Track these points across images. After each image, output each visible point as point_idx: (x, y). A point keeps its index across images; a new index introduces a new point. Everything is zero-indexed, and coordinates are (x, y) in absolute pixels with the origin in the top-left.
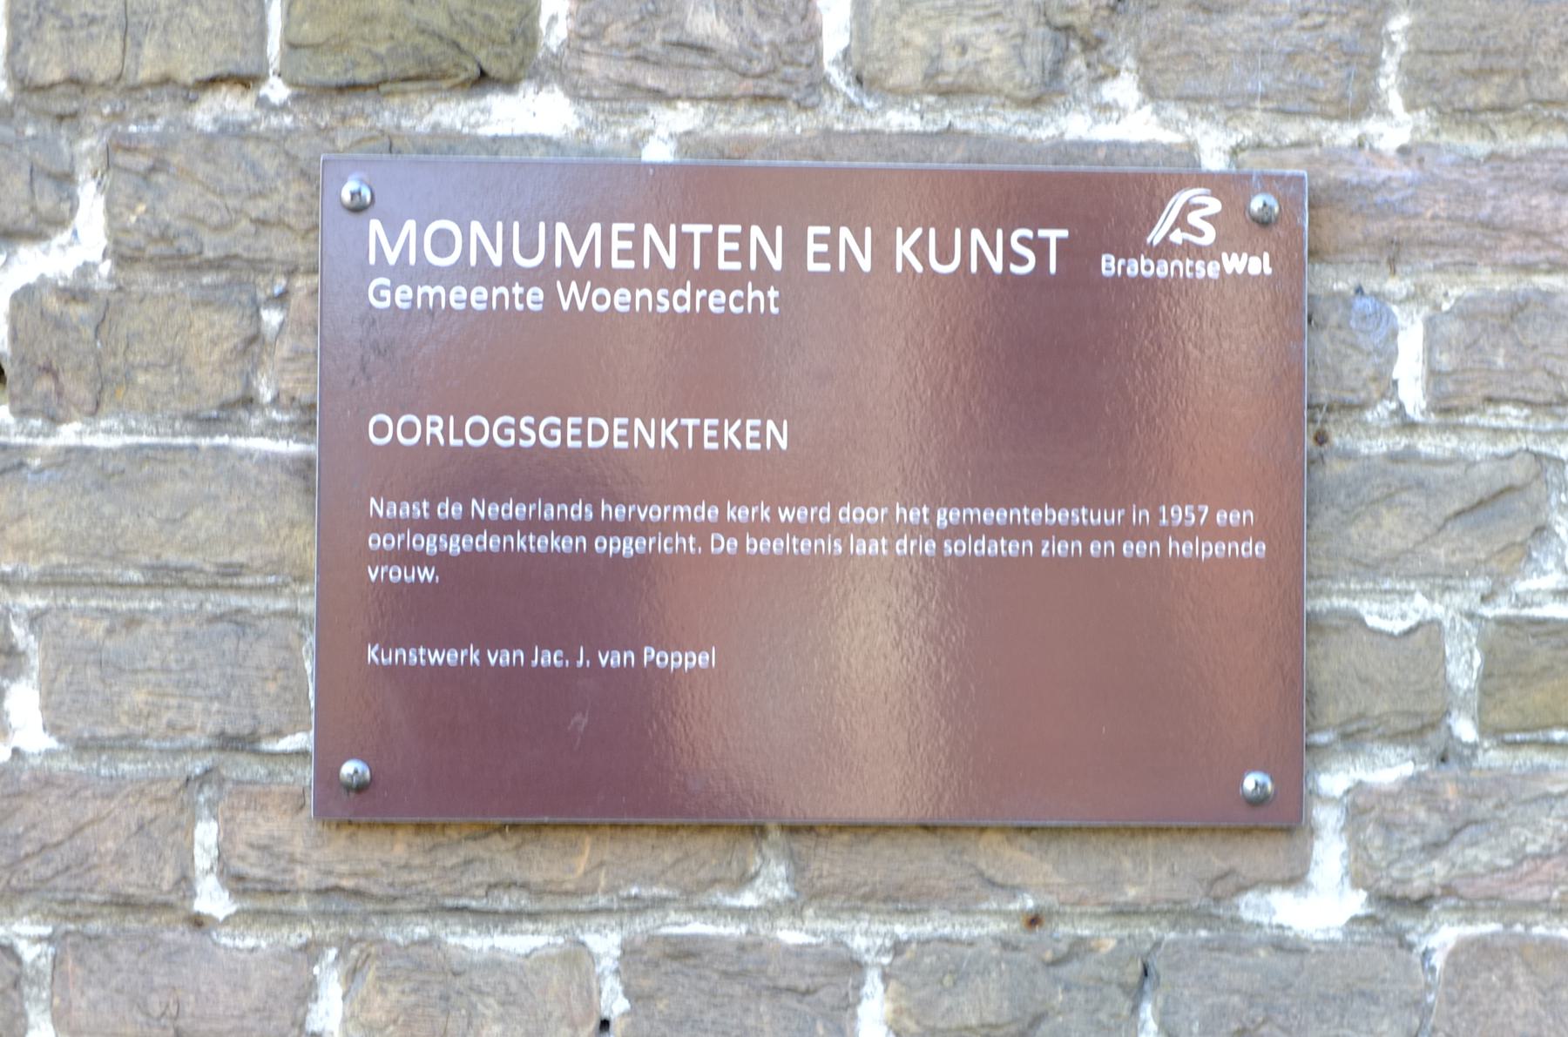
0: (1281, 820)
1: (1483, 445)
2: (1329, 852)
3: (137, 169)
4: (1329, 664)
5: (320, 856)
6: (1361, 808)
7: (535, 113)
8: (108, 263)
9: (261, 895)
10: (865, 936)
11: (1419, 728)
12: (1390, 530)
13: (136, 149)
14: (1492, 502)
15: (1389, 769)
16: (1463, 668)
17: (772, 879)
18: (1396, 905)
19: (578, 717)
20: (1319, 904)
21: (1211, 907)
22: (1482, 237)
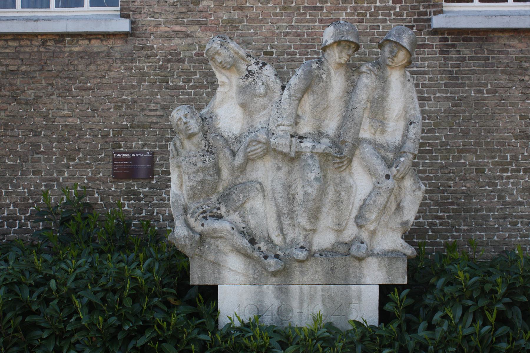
0: (153, 178)
1: (161, 163)
2: (155, 180)
3: (105, 152)
4: (155, 172)
5: (113, 180)
6: (156, 178)
7: (122, 149)
8: (510, 317)
9: (111, 182)
10: (135, 183)
11: (158, 174)
12: (157, 166)
13: (264, 199)
14: (161, 165)
15: (157, 176)
16: (160, 172)
17: (131, 181)
18: (157, 182)
19: (430, 348)
20: (154, 182)
21: (150, 182)
22: (161, 154)
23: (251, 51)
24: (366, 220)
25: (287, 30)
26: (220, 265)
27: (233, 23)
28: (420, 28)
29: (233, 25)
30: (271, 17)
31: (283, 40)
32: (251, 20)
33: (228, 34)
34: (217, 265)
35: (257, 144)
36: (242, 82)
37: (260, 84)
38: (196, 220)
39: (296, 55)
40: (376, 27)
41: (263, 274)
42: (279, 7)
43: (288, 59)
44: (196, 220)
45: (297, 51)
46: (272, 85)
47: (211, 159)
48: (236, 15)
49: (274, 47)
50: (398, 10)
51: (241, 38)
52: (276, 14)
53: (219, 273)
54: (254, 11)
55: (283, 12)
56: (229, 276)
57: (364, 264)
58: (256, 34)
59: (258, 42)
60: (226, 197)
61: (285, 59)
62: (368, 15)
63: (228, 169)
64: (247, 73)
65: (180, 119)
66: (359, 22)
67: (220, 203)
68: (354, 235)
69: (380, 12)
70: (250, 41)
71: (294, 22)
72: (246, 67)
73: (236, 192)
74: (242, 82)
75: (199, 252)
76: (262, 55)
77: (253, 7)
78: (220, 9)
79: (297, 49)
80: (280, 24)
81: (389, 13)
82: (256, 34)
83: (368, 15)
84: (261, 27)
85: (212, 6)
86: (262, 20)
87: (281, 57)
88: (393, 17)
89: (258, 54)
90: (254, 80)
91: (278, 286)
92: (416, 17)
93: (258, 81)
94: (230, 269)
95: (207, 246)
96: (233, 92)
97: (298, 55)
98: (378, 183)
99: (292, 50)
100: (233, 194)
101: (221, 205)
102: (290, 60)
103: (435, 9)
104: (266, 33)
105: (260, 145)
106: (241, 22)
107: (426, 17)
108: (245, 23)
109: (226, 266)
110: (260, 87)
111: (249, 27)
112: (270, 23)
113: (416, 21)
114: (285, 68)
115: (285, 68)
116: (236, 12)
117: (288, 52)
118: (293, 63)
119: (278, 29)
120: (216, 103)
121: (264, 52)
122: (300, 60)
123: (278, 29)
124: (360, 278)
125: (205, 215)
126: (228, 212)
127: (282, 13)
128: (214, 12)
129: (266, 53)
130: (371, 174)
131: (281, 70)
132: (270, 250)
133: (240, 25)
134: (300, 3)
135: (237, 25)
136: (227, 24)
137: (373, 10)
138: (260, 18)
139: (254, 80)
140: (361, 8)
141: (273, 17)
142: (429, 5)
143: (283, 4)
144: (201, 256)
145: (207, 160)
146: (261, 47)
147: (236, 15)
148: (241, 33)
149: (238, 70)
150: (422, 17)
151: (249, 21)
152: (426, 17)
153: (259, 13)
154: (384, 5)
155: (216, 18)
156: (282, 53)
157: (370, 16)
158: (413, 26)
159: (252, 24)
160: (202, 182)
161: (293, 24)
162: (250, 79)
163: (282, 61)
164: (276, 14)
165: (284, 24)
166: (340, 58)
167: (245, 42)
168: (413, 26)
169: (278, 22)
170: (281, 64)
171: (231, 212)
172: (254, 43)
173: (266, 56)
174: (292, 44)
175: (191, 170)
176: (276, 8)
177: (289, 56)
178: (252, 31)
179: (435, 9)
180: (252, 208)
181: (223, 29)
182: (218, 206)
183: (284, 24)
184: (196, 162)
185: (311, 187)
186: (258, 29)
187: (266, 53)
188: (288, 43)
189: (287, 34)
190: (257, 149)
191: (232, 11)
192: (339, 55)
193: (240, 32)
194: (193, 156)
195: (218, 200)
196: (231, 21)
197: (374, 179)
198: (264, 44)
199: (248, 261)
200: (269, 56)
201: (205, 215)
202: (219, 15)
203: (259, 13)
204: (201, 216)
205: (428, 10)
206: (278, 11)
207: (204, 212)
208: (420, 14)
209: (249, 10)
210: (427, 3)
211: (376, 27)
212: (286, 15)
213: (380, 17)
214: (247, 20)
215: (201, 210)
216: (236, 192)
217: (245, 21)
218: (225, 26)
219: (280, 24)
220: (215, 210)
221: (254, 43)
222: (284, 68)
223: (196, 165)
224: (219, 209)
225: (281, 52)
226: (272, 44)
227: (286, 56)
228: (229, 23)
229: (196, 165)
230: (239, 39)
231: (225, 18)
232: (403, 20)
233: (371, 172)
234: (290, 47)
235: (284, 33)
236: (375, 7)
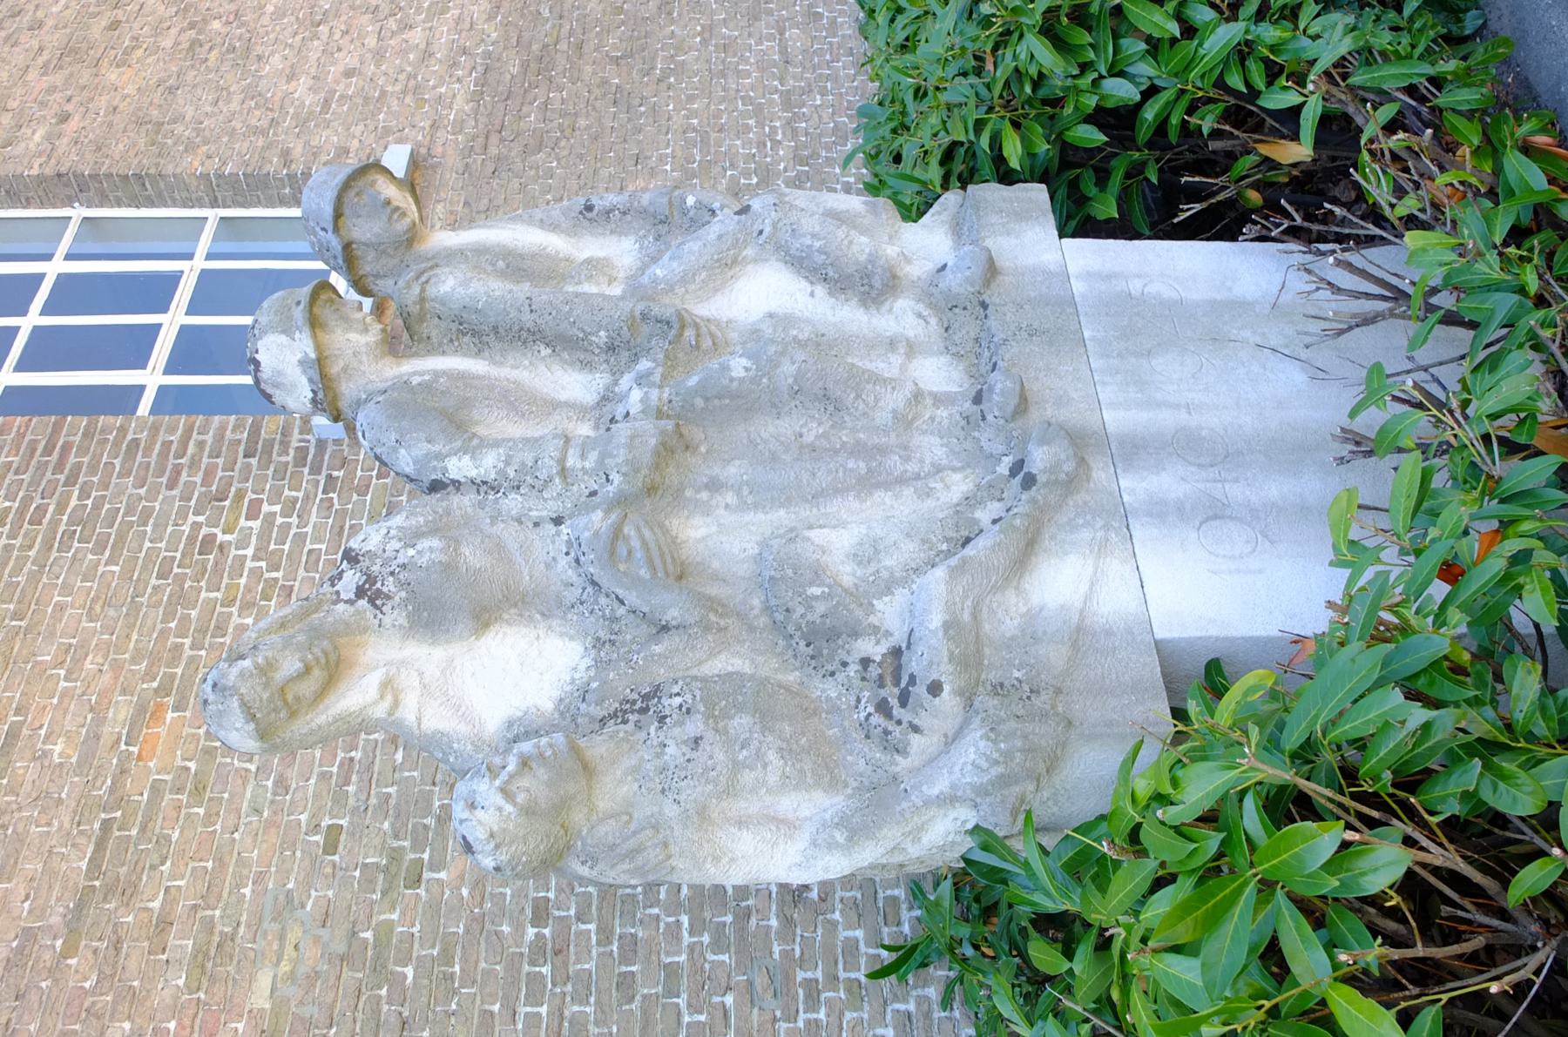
23: (313, 893)
24: (873, 259)
25: (270, 784)
26: (1079, 629)
27: (206, 955)
28: (338, 463)
29: (212, 954)
30: (215, 831)
31: (299, 795)
32: (209, 896)
33: (239, 971)
34: (1082, 636)
35: (627, 539)
36: (394, 616)
37: (411, 552)
38: (915, 729)
39: (352, 759)
40: (313, 557)
41: (1085, 503)
42: (189, 806)
43: (361, 780)
44: (915, 729)
45: (341, 755)
46: (421, 519)
47: (676, 689)
48: (183, 944)
49: (314, 822)
50: (277, 508)
51: (265, 925)
52: (210, 818)
53: (1109, 633)
54: (181, 883)
55: (208, 794)
56: (1115, 599)
57: (1003, 262)
58: (259, 879)
59: (289, 872)
60: (821, 640)
61: (360, 790)
62: (274, 575)
63: (712, 655)
64: (363, 603)
65: (505, 792)
66: (290, 595)
67: (845, 664)
68: (921, 307)
69: (272, 547)
70: (281, 898)
71: (247, 765)
72: (341, 607)
73: (800, 610)
74: (394, 616)
75: (1044, 697)
76: (336, 858)
77: (167, 889)
78: (146, 998)
79: (335, 756)
80: (245, 804)
81: (280, 527)
82: (259, 879)
83: (274, 575)
84: (241, 862)
85: (127, 1025)
86: (221, 862)
87: (352, 802)
88: (294, 520)
89: (329, 870)
90: (392, 573)
91: (1119, 465)
92: (306, 470)
93: (401, 560)
94: (1087, 598)
95: (1017, 674)
96: (426, 656)
97: (353, 754)
98: (761, 232)
99: (335, 770)
100: (809, 617)
101: (849, 660)
102: (366, 777)
103: (296, 431)
104: (265, 846)
105: (629, 530)
106: (209, 925)
107: (312, 451)
108: (217, 912)
109: (1078, 604)
110: (419, 552)
111: (234, 898)
112: (236, 835)
113: (316, 470)
114: (389, 790)
115: (389, 790)
116: (172, 942)
117: (341, 781)
118: (376, 768)
119: (258, 812)
120: (463, 729)
121: (326, 852)
122: (369, 749)
123: (258, 812)
124: (1049, 274)
125: (894, 702)
126: (876, 630)
127: (211, 799)
128: (152, 1019)
129: (331, 847)
130: (735, 262)
131: (392, 802)
132: (998, 494)
133: (219, 928)
134: (192, 747)
135: (216, 939)
136: (204, 973)
137: (263, 564)
138: (210, 865)
139: (392, 573)
140: (250, 591)
141: (218, 827)
142: (282, 443)
143: (184, 797)
144: (1058, 691)
145: (677, 701)
146: (307, 862)
147: (183, 944)
148: (248, 926)
149: (353, 629)
150: (310, 457)
151: (212, 901)
152: (312, 451)
153: (194, 869)
154: (254, 539)
155: (175, 1011)
156: (340, 798)
157: (277, 570)
158: (330, 477)
159: (225, 895)
160: (762, 717)
161: (253, 768)
162: (390, 586)
163: (363, 798)
164: (210, 818)
165: (248, 795)
166: (366, 330)
167: (280, 914)
168: (330, 477)
169: (238, 811)
170: (373, 801)
171: (873, 620)
172: (290, 886)
173: (341, 847)
174: (316, 770)
175: (720, 756)
176: (189, 815)
177: (354, 778)
178: (247, 891)
179: (296, 431)
180: (857, 557)
181: (219, 990)
182: (853, 669)
183: (248, 795)
184: (684, 742)
185: (777, 366)
186: (245, 872)
187: (331, 847)
188: (312, 781)
189: (282, 785)
190: (644, 543)
191: (164, 957)
192: (356, 331)
193: (242, 930)
194: (658, 756)
195: (832, 674)
196: (199, 961)
197: (749, 252)
198: (298, 854)
199: (1046, 542)
200: (343, 837)
201: (894, 702)
202: (168, 1001)
203: (194, 869)
204: (897, 711)
205: (295, 444)
206: (201, 811)
207: (883, 708)
208: (301, 459)
209: (175, 901)
210: (276, 447)
211: (313, 557)
212: (219, 787)
213: (286, 547)
214: (208, 908)
215: (877, 719)
216: (800, 610)
217: (209, 913)
218: (213, 979)
219: (245, 804)
220: (874, 671)
221: (290, 886)
222: (389, 795)
223: (697, 741)
224: (865, 662)
225: (335, 801)
226: (304, 829)
227: (351, 789)
228: (203, 966)
229: (697, 741)
230: (265, 933)
231: (181, 982)
232: (307, 497)
233: (726, 265)
234: (324, 777)
235: (275, 794)
236: (256, 558)
